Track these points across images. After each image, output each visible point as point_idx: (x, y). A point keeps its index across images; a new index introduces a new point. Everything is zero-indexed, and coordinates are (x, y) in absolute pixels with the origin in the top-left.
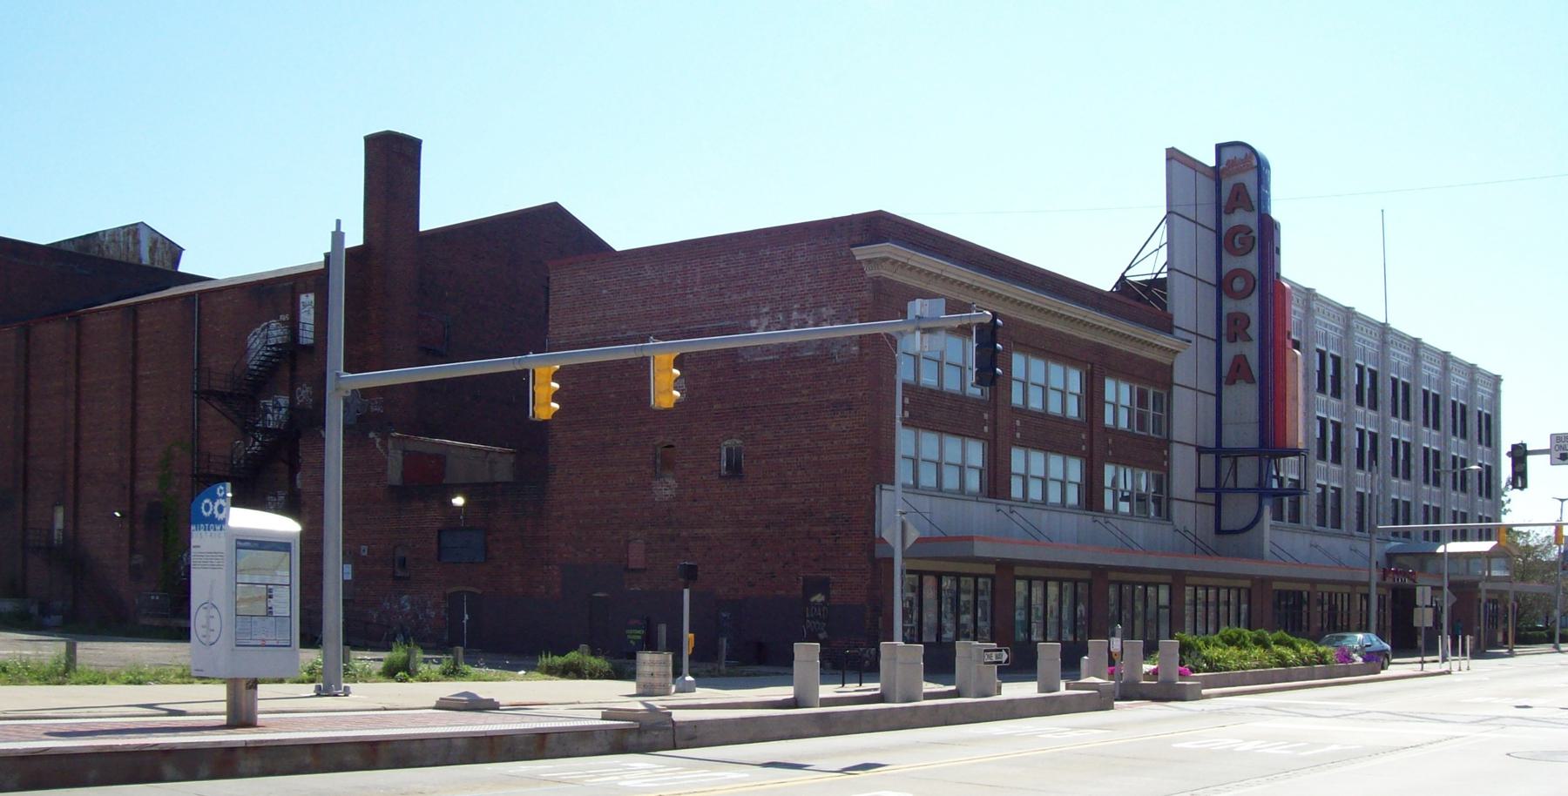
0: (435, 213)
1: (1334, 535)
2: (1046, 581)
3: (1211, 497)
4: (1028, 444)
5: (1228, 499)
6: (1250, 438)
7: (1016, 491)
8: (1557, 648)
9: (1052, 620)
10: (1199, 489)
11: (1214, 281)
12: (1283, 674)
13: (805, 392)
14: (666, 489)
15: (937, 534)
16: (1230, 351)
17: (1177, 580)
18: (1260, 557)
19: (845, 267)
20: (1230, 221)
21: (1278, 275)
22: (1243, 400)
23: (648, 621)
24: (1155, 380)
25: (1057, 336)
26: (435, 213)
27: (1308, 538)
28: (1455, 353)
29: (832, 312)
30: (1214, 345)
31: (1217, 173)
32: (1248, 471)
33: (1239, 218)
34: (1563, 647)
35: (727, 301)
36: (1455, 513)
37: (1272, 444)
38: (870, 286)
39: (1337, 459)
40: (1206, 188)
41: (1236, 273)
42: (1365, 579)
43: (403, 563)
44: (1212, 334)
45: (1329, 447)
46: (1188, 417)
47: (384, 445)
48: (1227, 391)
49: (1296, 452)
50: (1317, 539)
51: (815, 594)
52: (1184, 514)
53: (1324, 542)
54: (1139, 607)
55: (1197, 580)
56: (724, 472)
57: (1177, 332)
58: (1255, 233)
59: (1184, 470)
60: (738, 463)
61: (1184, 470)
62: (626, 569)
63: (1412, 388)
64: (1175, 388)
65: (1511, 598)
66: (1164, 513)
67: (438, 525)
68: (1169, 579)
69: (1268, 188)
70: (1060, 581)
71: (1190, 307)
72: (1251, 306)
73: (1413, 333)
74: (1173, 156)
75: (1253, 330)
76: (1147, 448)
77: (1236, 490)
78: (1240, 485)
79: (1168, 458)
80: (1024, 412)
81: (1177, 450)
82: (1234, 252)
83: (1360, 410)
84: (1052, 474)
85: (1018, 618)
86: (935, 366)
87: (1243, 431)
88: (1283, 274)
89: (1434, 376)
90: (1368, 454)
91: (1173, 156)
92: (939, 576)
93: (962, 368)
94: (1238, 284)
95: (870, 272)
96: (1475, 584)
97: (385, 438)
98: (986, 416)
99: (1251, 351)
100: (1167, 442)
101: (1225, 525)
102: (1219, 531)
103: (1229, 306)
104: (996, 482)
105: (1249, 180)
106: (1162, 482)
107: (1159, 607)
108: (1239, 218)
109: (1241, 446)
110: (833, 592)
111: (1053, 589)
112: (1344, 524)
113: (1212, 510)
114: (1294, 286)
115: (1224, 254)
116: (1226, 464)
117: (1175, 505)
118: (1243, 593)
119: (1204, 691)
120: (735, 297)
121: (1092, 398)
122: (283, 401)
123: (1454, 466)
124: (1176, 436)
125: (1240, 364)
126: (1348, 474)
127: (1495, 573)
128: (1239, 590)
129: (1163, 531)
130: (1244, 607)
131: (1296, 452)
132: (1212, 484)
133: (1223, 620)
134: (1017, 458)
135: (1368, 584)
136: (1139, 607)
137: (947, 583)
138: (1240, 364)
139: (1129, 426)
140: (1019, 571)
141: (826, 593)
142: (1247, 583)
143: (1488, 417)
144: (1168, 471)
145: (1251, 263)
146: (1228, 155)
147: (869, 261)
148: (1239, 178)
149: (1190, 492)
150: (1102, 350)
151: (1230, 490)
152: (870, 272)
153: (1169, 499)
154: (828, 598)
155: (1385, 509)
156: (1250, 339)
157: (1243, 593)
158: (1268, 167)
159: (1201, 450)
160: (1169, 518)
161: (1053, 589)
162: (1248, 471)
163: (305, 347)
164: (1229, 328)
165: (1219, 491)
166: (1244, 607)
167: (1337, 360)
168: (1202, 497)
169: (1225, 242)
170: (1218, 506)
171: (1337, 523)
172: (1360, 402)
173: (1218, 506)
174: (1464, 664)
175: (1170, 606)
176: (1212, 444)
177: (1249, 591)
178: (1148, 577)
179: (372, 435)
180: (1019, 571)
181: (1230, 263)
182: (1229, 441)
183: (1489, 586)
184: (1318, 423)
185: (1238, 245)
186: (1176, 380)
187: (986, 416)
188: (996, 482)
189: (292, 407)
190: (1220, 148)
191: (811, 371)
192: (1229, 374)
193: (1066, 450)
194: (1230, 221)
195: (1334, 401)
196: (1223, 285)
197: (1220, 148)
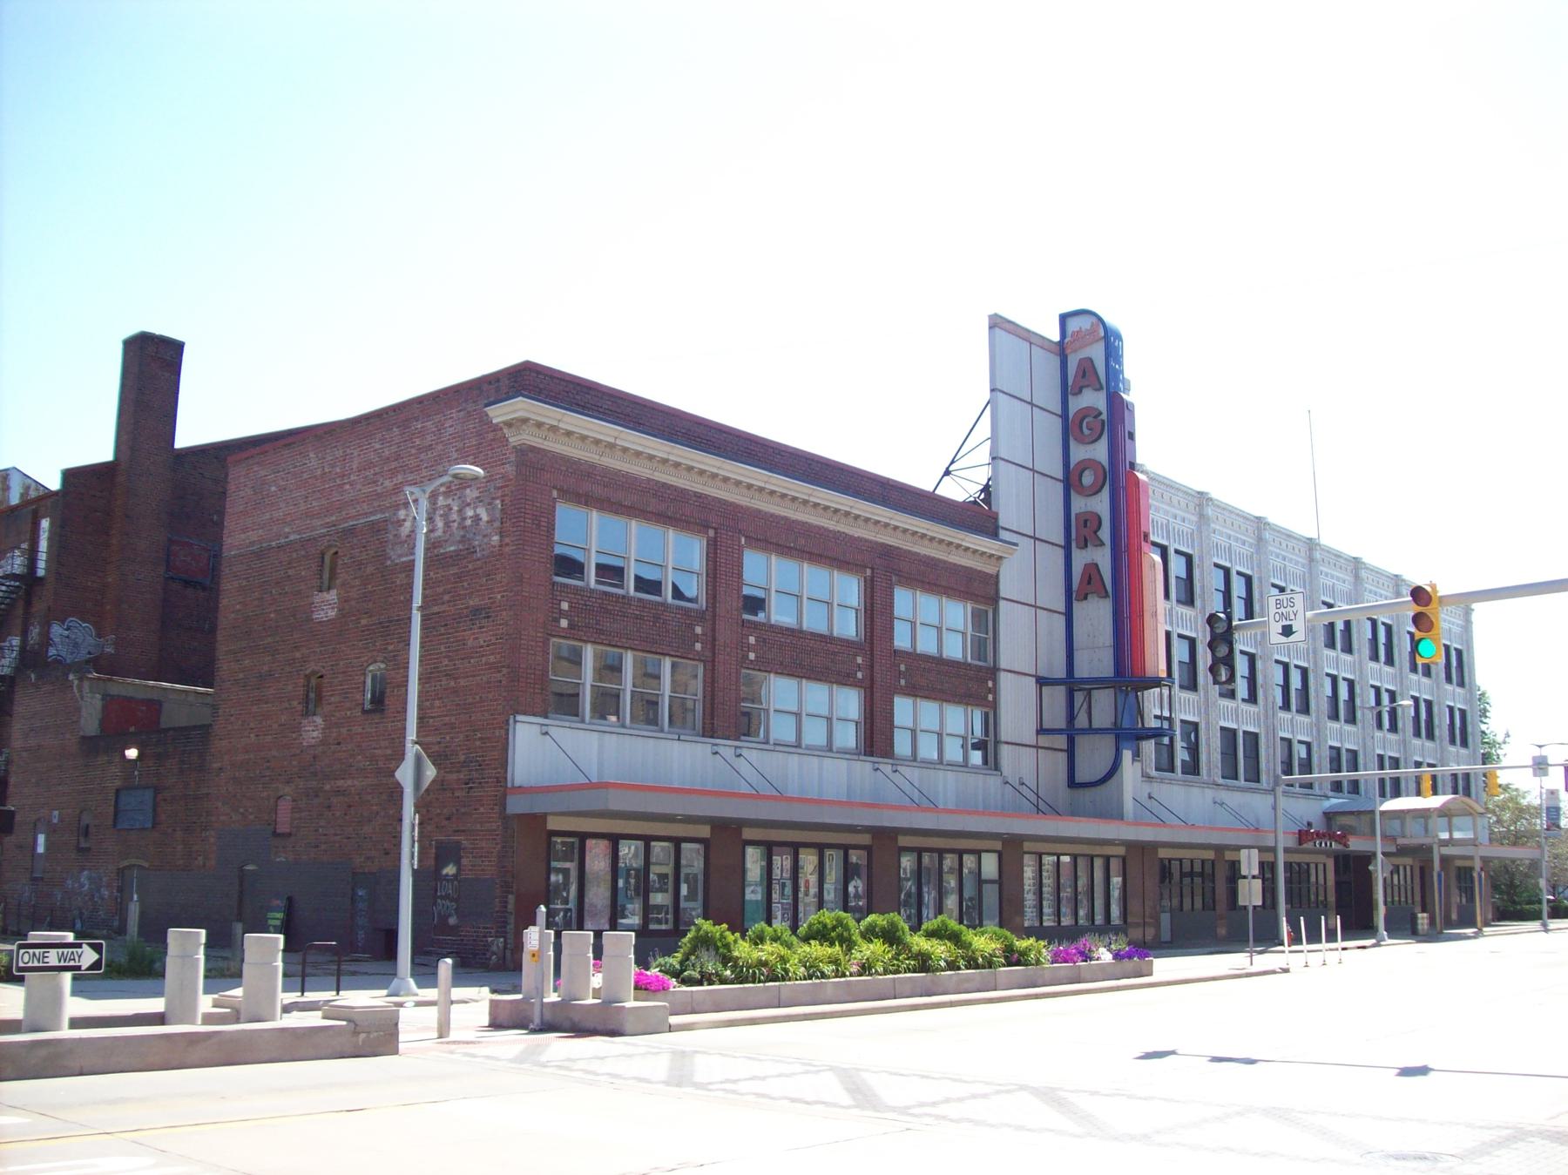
0: (191, 431)
1: (1228, 788)
2: (795, 848)
3: (1061, 742)
4: (913, 691)
5: (1082, 743)
6: (1106, 668)
7: (902, 745)
8: (1545, 925)
9: (1066, 893)
10: (1041, 731)
11: (1060, 475)
12: (869, 990)
13: (446, 597)
14: (313, 731)
15: (767, 790)
16: (1080, 558)
17: (1011, 848)
18: (1118, 815)
19: (491, 436)
20: (1076, 404)
21: (1132, 465)
22: (1096, 616)
23: (290, 899)
24: (981, 591)
25: (682, 495)
26: (191, 431)
27: (1209, 793)
28: (1274, 518)
29: (476, 494)
30: (1060, 553)
31: (1061, 350)
32: (1103, 707)
33: (1093, 399)
34: (1554, 924)
35: (379, 489)
36: (1381, 757)
37: (1129, 677)
38: (513, 458)
39: (1352, 719)
40: (1048, 367)
41: (1086, 465)
42: (1271, 843)
43: (86, 832)
44: (1059, 538)
45: (1342, 706)
46: (1025, 641)
47: (80, 688)
48: (1077, 607)
49: (1156, 682)
50: (1224, 795)
51: (446, 865)
52: (1018, 763)
53: (1234, 799)
54: (952, 882)
55: (1040, 847)
56: (368, 706)
57: (1003, 535)
58: (1104, 416)
59: (1018, 706)
60: (382, 693)
61: (1018, 706)
62: (275, 834)
63: (1395, 629)
64: (1002, 604)
65: (1478, 865)
66: (992, 763)
67: (118, 783)
68: (998, 845)
69: (1120, 363)
70: (821, 848)
71: (1030, 509)
72: (1101, 504)
73: (1350, 550)
74: (997, 324)
75: (1105, 533)
76: (970, 682)
77: (1091, 730)
78: (1096, 725)
79: (995, 691)
80: (913, 657)
81: (1005, 680)
82: (1082, 441)
83: (1448, 687)
84: (809, 707)
85: (749, 896)
86: (934, 632)
87: (1096, 660)
88: (1140, 459)
89: (1456, 629)
90: (1344, 708)
91: (997, 324)
92: (614, 839)
93: (964, 634)
94: (1088, 478)
95: (514, 439)
96: (1429, 849)
97: (81, 679)
98: (859, 660)
99: (1102, 558)
100: (994, 671)
101: (1081, 777)
102: (1072, 783)
103: (1079, 504)
104: (876, 738)
105: (1097, 353)
106: (991, 723)
107: (980, 882)
108: (1093, 399)
109: (1096, 675)
110: (464, 861)
111: (809, 860)
112: (1263, 777)
113: (1063, 757)
114: (1154, 478)
115: (1072, 443)
116: (1079, 697)
117: (1005, 750)
118: (1115, 865)
119: (673, 1020)
120: (387, 483)
121: (877, 613)
122: (16, 641)
123: (1378, 702)
124: (1004, 663)
125: (1092, 571)
126: (1318, 725)
127: (1457, 835)
128: (1107, 859)
129: (991, 784)
130: (1116, 881)
131: (1156, 682)
132: (1061, 723)
133: (808, 899)
134: (903, 709)
135: (1273, 850)
136: (952, 882)
137: (628, 850)
138: (1092, 571)
139: (965, 656)
140: (903, 841)
141: (458, 863)
142: (1121, 851)
143: (1459, 653)
144: (995, 705)
145: (1100, 451)
146: (1073, 325)
147: (509, 424)
148: (1084, 354)
149: (1029, 735)
150: (887, 552)
151: (1083, 731)
152: (514, 439)
153: (997, 742)
154: (459, 870)
155: (1321, 757)
156: (1102, 544)
157: (1115, 865)
158: (1119, 337)
159: (1042, 682)
160: (997, 767)
161: (809, 860)
162: (1103, 704)
163: (41, 579)
164: (1079, 531)
165: (1071, 733)
166: (1116, 881)
167: (1389, 628)
168: (1044, 740)
169: (1072, 427)
170: (1071, 752)
171: (1254, 776)
172: (1375, 657)
173: (1071, 752)
174: (1315, 959)
175: (1000, 881)
176: (1061, 673)
177: (1124, 859)
178: (963, 844)
179: (71, 677)
180: (1027, 846)
181: (1079, 453)
182: (1082, 671)
183: (1446, 851)
184: (1372, 692)
185: (1086, 431)
186: (1002, 594)
187: (698, 630)
188: (876, 738)
189: (23, 648)
190: (1064, 318)
191: (453, 570)
192: (1079, 587)
193: (845, 679)
194: (1076, 404)
195: (1388, 669)
196: (1071, 481)
197: (1064, 318)
